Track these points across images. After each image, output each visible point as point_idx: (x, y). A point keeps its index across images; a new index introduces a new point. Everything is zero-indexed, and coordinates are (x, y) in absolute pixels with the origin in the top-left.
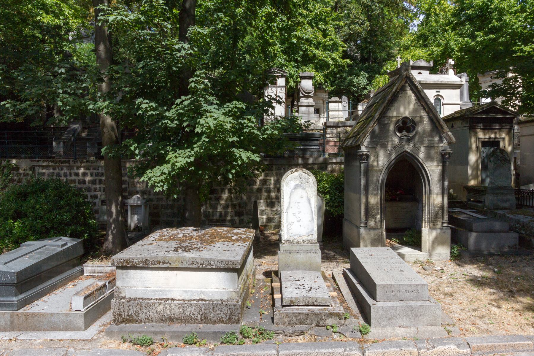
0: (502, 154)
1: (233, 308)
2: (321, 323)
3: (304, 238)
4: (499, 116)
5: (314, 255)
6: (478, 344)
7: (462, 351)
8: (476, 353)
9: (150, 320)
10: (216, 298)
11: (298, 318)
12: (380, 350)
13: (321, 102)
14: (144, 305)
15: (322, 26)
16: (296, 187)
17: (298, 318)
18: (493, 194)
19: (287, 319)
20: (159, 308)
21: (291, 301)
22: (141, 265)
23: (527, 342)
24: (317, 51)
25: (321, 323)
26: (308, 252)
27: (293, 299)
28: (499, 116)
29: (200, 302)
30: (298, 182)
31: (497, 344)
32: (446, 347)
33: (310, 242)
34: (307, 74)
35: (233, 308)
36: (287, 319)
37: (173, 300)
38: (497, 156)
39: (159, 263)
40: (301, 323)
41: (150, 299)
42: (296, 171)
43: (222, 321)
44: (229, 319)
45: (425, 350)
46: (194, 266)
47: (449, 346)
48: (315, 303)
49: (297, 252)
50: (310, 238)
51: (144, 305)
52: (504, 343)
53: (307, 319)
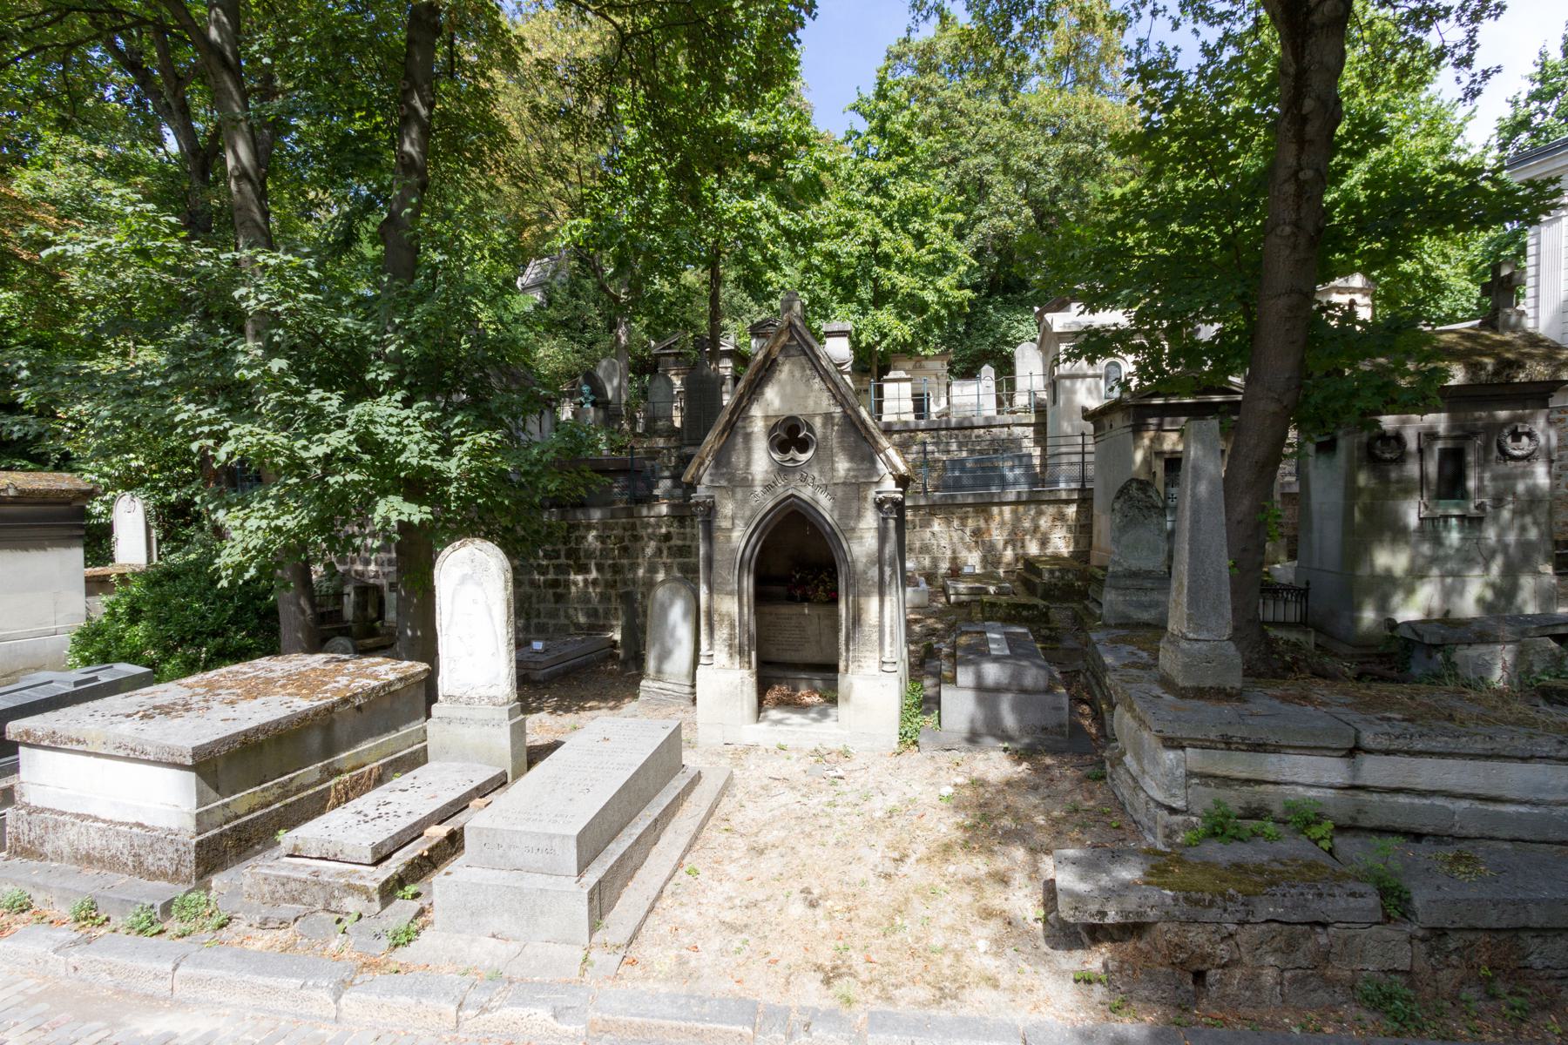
0: (1145, 491)
1: (182, 849)
2: (334, 906)
3: (483, 692)
4: (1217, 399)
5: (495, 731)
6: (606, 1016)
7: (565, 1027)
8: (599, 1039)
9: (59, 855)
10: (159, 824)
11: (288, 888)
12: (374, 998)
13: (934, 378)
14: (51, 824)
15: (916, 225)
16: (464, 579)
17: (288, 888)
18: (1117, 588)
19: (266, 888)
20: (72, 833)
21: (296, 847)
22: (46, 743)
23: (740, 1028)
24: (901, 278)
25: (334, 906)
26: (485, 723)
27: (299, 842)
28: (1217, 399)
29: (135, 830)
30: (467, 570)
31: (656, 1022)
32: (524, 1011)
33: (492, 701)
34: (836, 326)
35: (182, 849)
36: (266, 888)
37: (96, 819)
38: (1131, 498)
39: (78, 741)
40: (294, 900)
41: (63, 813)
42: (463, 545)
43: (164, 875)
44: (177, 872)
45: (474, 1013)
46: (122, 753)
47: (532, 1011)
48: (340, 856)
49: (463, 721)
50: (492, 692)
51: (51, 824)
52: (675, 1023)
53: (304, 891)
